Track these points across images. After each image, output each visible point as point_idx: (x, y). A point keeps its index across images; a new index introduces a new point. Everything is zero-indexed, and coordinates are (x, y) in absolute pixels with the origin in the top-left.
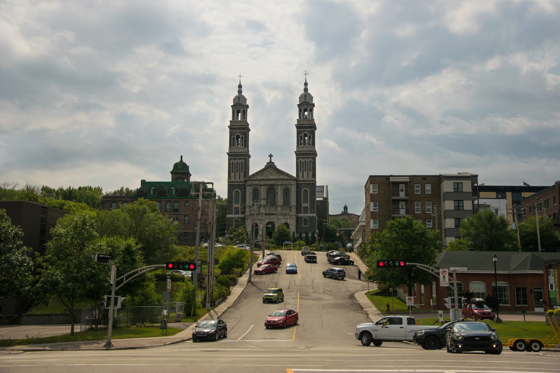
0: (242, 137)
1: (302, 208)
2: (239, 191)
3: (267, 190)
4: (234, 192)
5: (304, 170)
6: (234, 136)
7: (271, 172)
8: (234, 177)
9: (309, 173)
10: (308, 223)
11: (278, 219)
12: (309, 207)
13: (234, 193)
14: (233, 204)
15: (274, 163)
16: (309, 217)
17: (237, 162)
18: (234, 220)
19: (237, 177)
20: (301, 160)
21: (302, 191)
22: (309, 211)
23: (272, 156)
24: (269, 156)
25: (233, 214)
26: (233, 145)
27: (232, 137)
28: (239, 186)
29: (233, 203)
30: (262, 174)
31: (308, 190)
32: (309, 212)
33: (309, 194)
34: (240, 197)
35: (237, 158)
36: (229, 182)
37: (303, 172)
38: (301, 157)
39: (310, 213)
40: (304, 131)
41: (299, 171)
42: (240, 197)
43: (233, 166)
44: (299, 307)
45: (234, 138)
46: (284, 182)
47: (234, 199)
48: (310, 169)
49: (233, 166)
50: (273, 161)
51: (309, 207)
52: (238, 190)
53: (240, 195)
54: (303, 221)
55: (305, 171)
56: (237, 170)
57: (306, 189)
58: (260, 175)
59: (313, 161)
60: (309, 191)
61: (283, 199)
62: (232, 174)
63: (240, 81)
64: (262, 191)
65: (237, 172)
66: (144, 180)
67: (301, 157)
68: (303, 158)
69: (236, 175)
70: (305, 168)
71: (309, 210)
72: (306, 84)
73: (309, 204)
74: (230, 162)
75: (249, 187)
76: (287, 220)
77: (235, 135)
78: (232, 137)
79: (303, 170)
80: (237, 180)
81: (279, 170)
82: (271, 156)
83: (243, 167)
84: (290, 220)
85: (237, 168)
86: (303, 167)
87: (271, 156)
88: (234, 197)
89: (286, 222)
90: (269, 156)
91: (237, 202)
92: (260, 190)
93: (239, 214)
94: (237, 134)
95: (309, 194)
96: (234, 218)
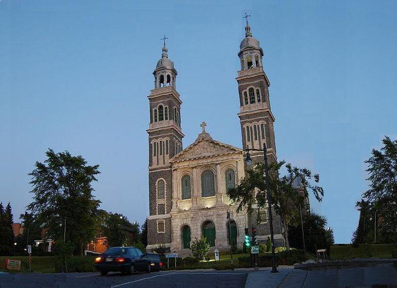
17: (155, 143)
18: (157, 223)
19: (161, 161)
27: (243, 92)
28: (162, 174)
40: (249, 85)
41: (247, 140)
48: (263, 134)
59: (266, 123)
62: (155, 159)
64: (195, 176)
68: (251, 122)
72: (247, 29)
74: (151, 143)
75: (175, 172)
78: (243, 92)
82: (204, 125)
90: (201, 125)
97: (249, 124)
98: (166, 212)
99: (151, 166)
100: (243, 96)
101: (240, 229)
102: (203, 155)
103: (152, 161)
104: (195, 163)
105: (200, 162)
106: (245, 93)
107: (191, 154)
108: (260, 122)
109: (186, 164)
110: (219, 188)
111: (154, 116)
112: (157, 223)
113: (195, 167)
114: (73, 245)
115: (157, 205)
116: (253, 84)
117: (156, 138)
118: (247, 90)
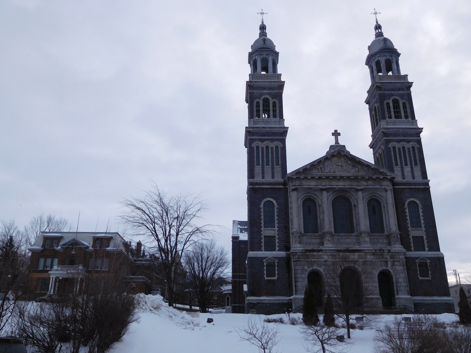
0: (273, 102)
1: (410, 239)
2: (274, 202)
3: (333, 201)
4: (262, 204)
5: (404, 164)
6: (258, 100)
7: (341, 164)
8: (261, 175)
9: (414, 169)
10: (430, 272)
12: (425, 237)
13: (262, 206)
14: (262, 229)
15: (344, 147)
16: (430, 258)
17: (267, 147)
18: (265, 264)
20: (395, 144)
21: (406, 204)
22: (426, 245)
23: (339, 134)
24: (333, 134)
25: (262, 250)
26: (273, 115)
29: (261, 227)
30: (321, 168)
31: (418, 202)
32: (427, 249)
33: (421, 211)
34: (276, 214)
35: (266, 137)
36: (250, 184)
38: (395, 138)
40: (392, 95)
41: (394, 164)
42: (276, 214)
43: (258, 153)
44: (419, 157)
45: (258, 103)
47: (262, 217)
49: (258, 153)
50: (341, 143)
51: (425, 237)
52: (271, 200)
53: (276, 210)
54: (418, 268)
55: (406, 165)
56: (268, 160)
57: (412, 199)
58: (318, 169)
60: (420, 206)
61: (368, 219)
62: (258, 169)
63: (263, 20)
65: (268, 164)
66: (429, 181)
67: (395, 138)
68: (398, 141)
69: (265, 171)
71: (425, 243)
73: (278, 231)
79: (401, 163)
80: (268, 179)
81: (358, 160)
83: (280, 156)
85: (267, 156)
86: (401, 158)
88: (262, 214)
90: (333, 134)
91: (269, 223)
92: (318, 199)
93: (275, 250)
94: (263, 97)
95: (421, 211)
96: (265, 258)
98: (277, 248)
99: (264, 179)
100: (386, 107)
102: (338, 174)
103: (262, 171)
104: (325, 184)
108: (411, 143)
109: (313, 184)
110: (389, 212)
111: (278, 111)
112: (265, 264)
113: (326, 190)
115: (262, 237)
116: (269, 94)
117: (260, 140)
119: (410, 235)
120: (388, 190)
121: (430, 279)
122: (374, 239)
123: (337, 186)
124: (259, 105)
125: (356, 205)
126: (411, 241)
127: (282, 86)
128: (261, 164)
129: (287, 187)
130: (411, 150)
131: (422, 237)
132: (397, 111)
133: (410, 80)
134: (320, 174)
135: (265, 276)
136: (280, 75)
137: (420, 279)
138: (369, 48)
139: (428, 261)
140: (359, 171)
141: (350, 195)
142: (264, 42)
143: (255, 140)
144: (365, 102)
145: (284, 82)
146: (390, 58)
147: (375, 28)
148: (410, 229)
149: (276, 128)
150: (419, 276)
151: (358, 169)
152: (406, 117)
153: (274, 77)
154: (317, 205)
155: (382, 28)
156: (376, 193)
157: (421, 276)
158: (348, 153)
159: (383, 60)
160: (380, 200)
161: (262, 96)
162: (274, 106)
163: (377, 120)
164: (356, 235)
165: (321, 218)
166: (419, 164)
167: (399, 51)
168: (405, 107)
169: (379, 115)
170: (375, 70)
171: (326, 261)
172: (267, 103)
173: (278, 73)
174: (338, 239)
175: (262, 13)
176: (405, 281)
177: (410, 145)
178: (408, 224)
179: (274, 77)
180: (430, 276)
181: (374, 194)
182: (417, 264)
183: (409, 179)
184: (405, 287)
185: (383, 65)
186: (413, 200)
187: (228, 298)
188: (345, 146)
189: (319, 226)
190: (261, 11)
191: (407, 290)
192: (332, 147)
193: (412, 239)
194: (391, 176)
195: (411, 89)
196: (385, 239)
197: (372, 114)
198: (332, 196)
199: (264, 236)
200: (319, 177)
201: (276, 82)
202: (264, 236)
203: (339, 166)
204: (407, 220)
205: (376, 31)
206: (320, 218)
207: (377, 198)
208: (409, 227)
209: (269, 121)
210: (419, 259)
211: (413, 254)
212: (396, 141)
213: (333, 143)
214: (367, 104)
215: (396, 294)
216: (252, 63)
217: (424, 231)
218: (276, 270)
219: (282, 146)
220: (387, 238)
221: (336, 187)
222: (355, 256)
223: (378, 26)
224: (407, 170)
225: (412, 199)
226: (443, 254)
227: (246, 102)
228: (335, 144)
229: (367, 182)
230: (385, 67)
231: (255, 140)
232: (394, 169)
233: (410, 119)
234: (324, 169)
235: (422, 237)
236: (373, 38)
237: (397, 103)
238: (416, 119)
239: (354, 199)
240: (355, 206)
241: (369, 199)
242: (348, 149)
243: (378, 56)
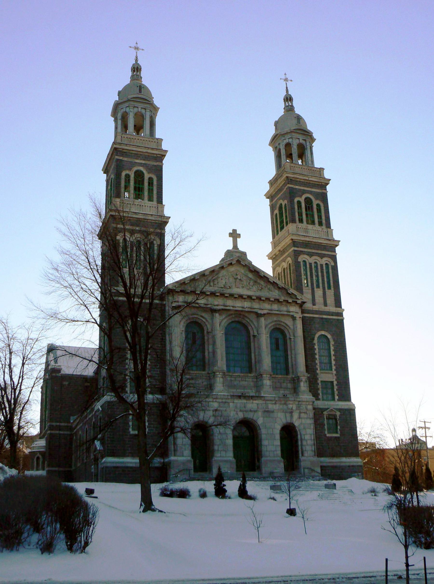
1: (318, 384)
5: (326, 288)
6: (127, 172)
7: (239, 278)
11: (268, 412)
12: (335, 383)
15: (244, 254)
16: (340, 410)
21: (316, 338)
24: (231, 235)
31: (329, 336)
32: (337, 397)
37: (313, 289)
38: (306, 250)
39: (339, 400)
40: (304, 192)
46: (275, 307)
48: (329, 282)
50: (241, 247)
51: (335, 383)
54: (326, 422)
60: (332, 343)
67: (306, 250)
68: (311, 255)
70: (318, 281)
73: (336, 375)
76: (292, 416)
77: (130, 169)
78: (124, 174)
81: (262, 275)
84: (300, 418)
87: (234, 235)
89: (289, 420)
90: (231, 235)
94: (135, 169)
97: (306, 256)
101: (304, 443)
105: (230, 303)
106: (128, 176)
107: (212, 284)
111: (323, 217)
114: (306, 471)
118: (302, 200)
119: (318, 379)
120: (297, 318)
121: (338, 435)
122: (276, 383)
123: (233, 307)
124: (129, 180)
125: (256, 336)
126: (320, 386)
127: (163, 157)
128: (128, 267)
129: (165, 303)
130: (324, 268)
131: (332, 382)
132: (139, 188)
133: (164, 147)
134: (212, 289)
135: (326, 432)
136: (321, 170)
137: (71, 417)
138: (119, 93)
139: (338, 414)
140: (262, 289)
141: (248, 320)
142: (140, 91)
143: (302, 253)
144: (265, 195)
145: (166, 151)
146: (143, 111)
147: (284, 99)
148: (318, 371)
149: (153, 216)
150: (326, 432)
151: (261, 286)
152: (320, 224)
153: (152, 141)
154: (205, 332)
155: (283, 101)
156: (282, 322)
157: (328, 433)
158: (250, 263)
159: (295, 143)
160: (287, 333)
161: (134, 167)
162: (151, 183)
163: (282, 222)
164: (254, 376)
165: (211, 350)
166: (332, 289)
167: (315, 136)
168: (319, 210)
169: (286, 216)
170: (284, 155)
171: (216, 410)
172: (309, 205)
173: (157, 136)
174: (231, 380)
175: (137, 48)
176: (313, 438)
177: (324, 261)
178: (317, 364)
179: (152, 141)
180: (339, 432)
181: (278, 323)
182: (325, 417)
183: (319, 306)
184: (312, 446)
185: (295, 150)
186: (324, 334)
187: (38, 458)
188: (246, 253)
189: (207, 361)
190: (135, 45)
191: (313, 449)
192: (228, 253)
193: (320, 384)
194: (303, 301)
195: (327, 187)
196: (289, 383)
197: (275, 213)
198: (225, 320)
199: (321, 381)
200: (210, 293)
201: (155, 150)
202: (321, 381)
203: (237, 280)
204: (316, 359)
205: (285, 103)
206: (208, 350)
207: (282, 328)
208: (317, 369)
209: (142, 204)
210: (328, 410)
211: (320, 404)
212: (307, 253)
213: (230, 247)
214: (104, 173)
215: (300, 455)
216: (119, 116)
217: (334, 375)
218: (146, 421)
219: (333, 264)
220: (292, 382)
221: (231, 308)
222: (252, 405)
223: (289, 98)
224: (319, 293)
225: (323, 333)
226: (354, 405)
227: (103, 172)
228: (233, 249)
229: (271, 305)
230: (297, 153)
231: (302, 253)
232: (304, 290)
233: (324, 227)
234: (217, 281)
235: (332, 382)
236: (127, 81)
237: (311, 204)
238: (332, 228)
239: (253, 326)
240: (254, 336)
241: (273, 328)
242: (249, 257)
243: (288, 137)
